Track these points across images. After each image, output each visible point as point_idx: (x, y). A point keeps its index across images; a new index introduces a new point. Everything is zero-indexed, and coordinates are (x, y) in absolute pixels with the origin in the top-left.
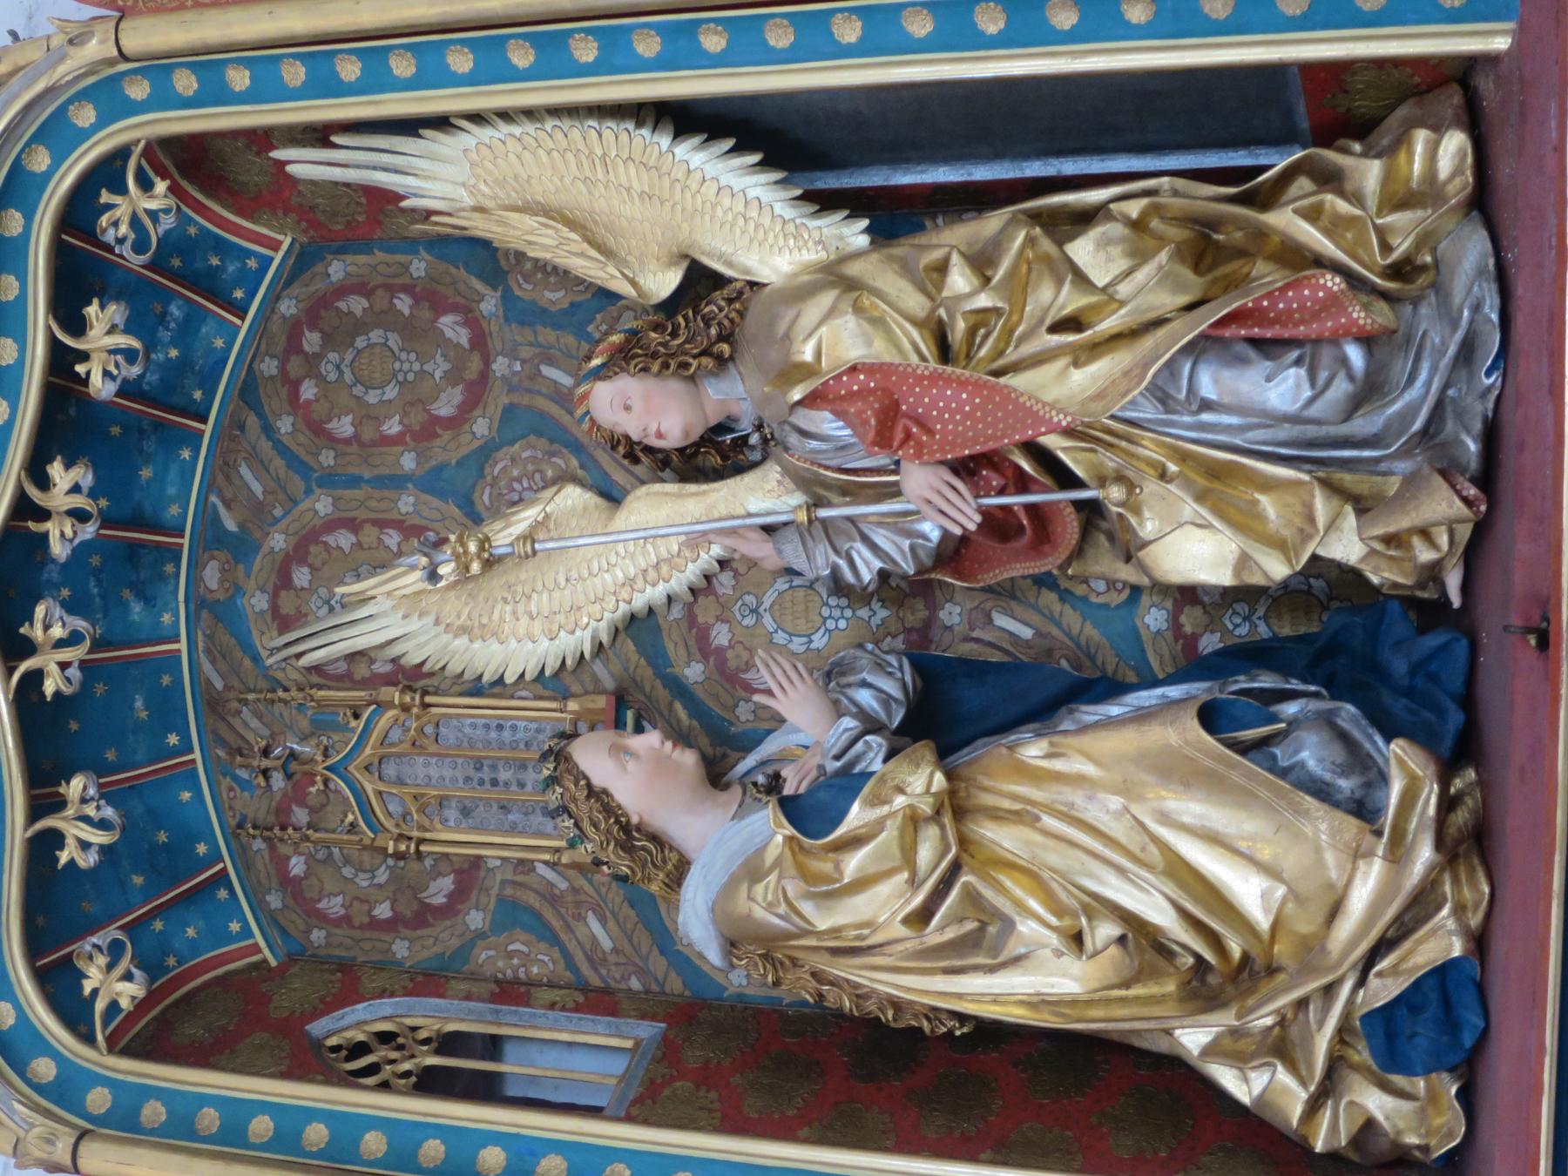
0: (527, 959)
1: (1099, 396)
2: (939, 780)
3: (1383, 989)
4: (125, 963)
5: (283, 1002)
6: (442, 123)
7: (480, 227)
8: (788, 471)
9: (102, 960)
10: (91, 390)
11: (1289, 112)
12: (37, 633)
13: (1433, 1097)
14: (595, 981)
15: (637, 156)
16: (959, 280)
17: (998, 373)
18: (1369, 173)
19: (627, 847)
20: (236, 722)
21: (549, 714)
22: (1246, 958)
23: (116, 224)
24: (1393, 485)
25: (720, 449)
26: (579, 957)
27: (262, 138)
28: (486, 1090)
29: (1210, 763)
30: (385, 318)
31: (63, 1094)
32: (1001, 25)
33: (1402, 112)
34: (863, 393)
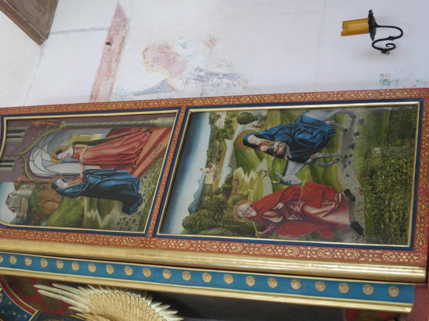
6: (85, 286)
15: (140, 306)
32: (254, 284)
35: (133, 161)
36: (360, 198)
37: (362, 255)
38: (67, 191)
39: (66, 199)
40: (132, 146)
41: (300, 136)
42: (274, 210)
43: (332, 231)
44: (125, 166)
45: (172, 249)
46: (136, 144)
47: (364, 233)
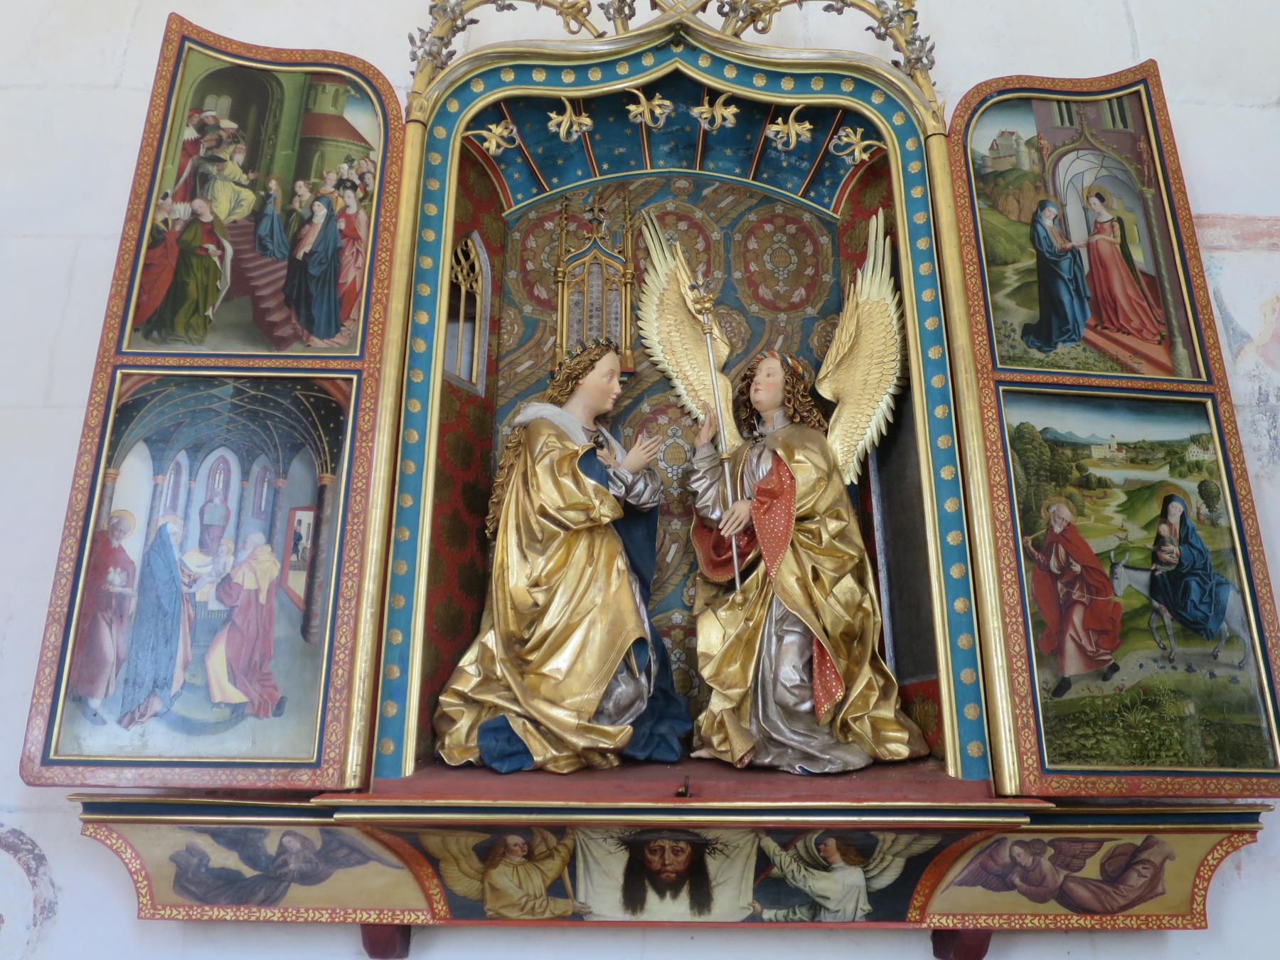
0: (510, 333)
1: (784, 589)
2: (606, 520)
3: (517, 725)
4: (505, 145)
5: (486, 219)
6: (898, 287)
7: (849, 306)
8: (739, 448)
9: (505, 133)
10: (769, 126)
11: (912, 675)
12: (657, 102)
13: (467, 750)
14: (501, 365)
16: (833, 525)
17: (792, 544)
18: (888, 712)
19: (569, 378)
20: (614, 196)
21: (624, 340)
22: (529, 662)
23: (847, 136)
24: (746, 725)
25: (751, 417)
26: (513, 357)
27: (888, 203)
28: (453, 315)
29: (619, 643)
30: (803, 263)
31: (443, 116)
33: (915, 727)
34: (781, 483)
35: (1107, 324)
36: (1108, 687)
37: (1023, 699)
38: (1039, 228)
39: (1027, 230)
40: (1132, 316)
41: (1194, 585)
42: (1067, 559)
43: (1051, 651)
44: (1097, 313)
45: (982, 414)
46: (1136, 323)
47: (1056, 699)
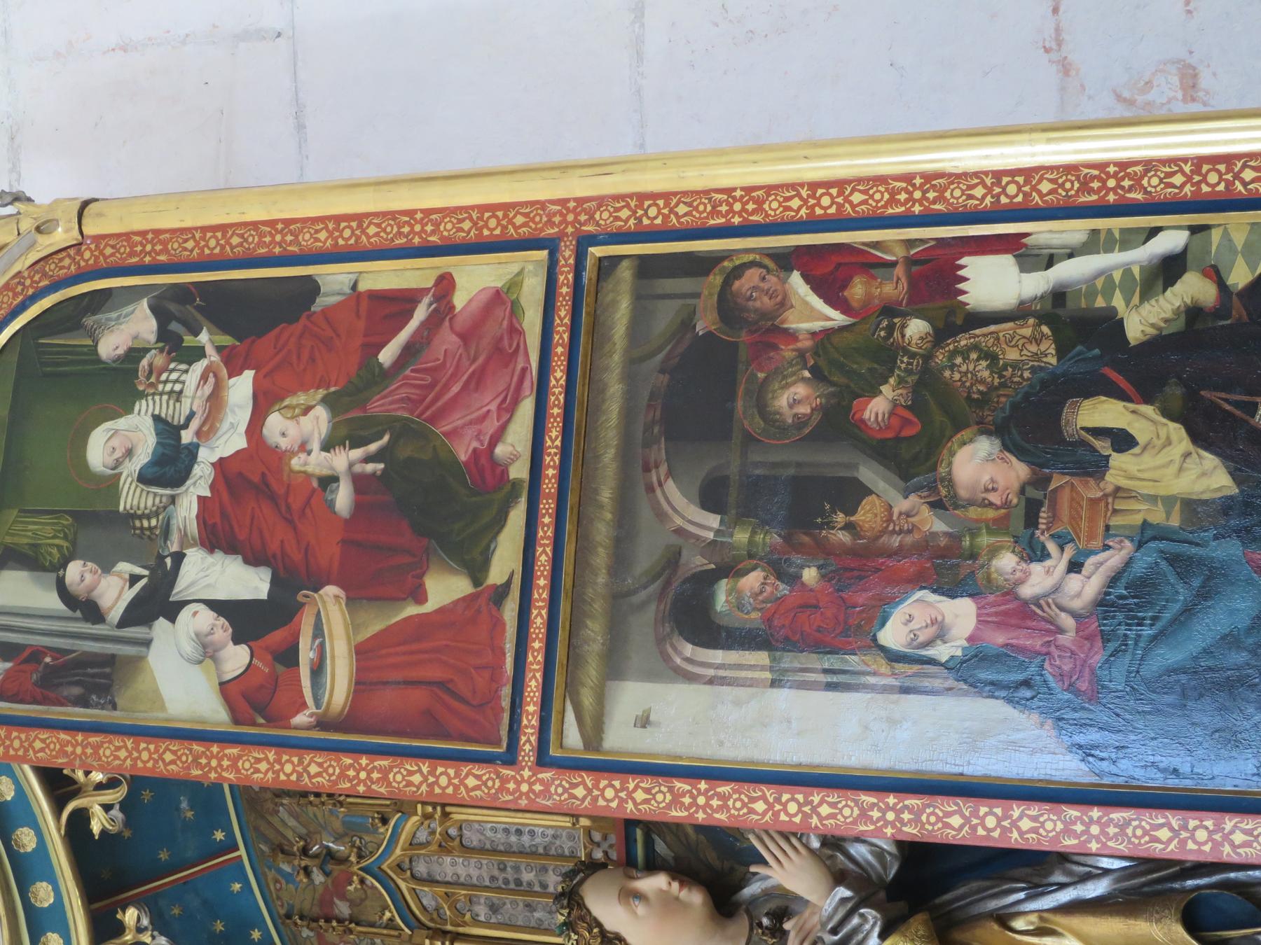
20: (275, 820)
